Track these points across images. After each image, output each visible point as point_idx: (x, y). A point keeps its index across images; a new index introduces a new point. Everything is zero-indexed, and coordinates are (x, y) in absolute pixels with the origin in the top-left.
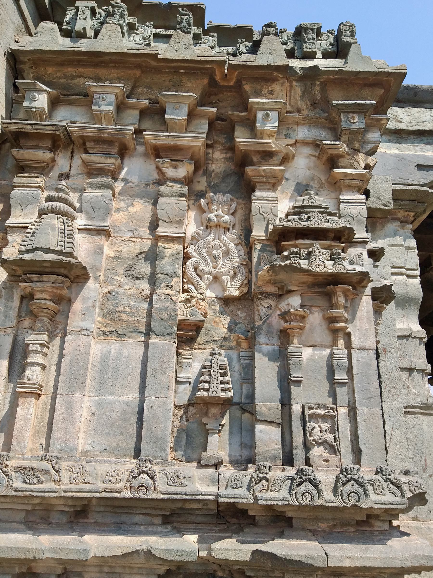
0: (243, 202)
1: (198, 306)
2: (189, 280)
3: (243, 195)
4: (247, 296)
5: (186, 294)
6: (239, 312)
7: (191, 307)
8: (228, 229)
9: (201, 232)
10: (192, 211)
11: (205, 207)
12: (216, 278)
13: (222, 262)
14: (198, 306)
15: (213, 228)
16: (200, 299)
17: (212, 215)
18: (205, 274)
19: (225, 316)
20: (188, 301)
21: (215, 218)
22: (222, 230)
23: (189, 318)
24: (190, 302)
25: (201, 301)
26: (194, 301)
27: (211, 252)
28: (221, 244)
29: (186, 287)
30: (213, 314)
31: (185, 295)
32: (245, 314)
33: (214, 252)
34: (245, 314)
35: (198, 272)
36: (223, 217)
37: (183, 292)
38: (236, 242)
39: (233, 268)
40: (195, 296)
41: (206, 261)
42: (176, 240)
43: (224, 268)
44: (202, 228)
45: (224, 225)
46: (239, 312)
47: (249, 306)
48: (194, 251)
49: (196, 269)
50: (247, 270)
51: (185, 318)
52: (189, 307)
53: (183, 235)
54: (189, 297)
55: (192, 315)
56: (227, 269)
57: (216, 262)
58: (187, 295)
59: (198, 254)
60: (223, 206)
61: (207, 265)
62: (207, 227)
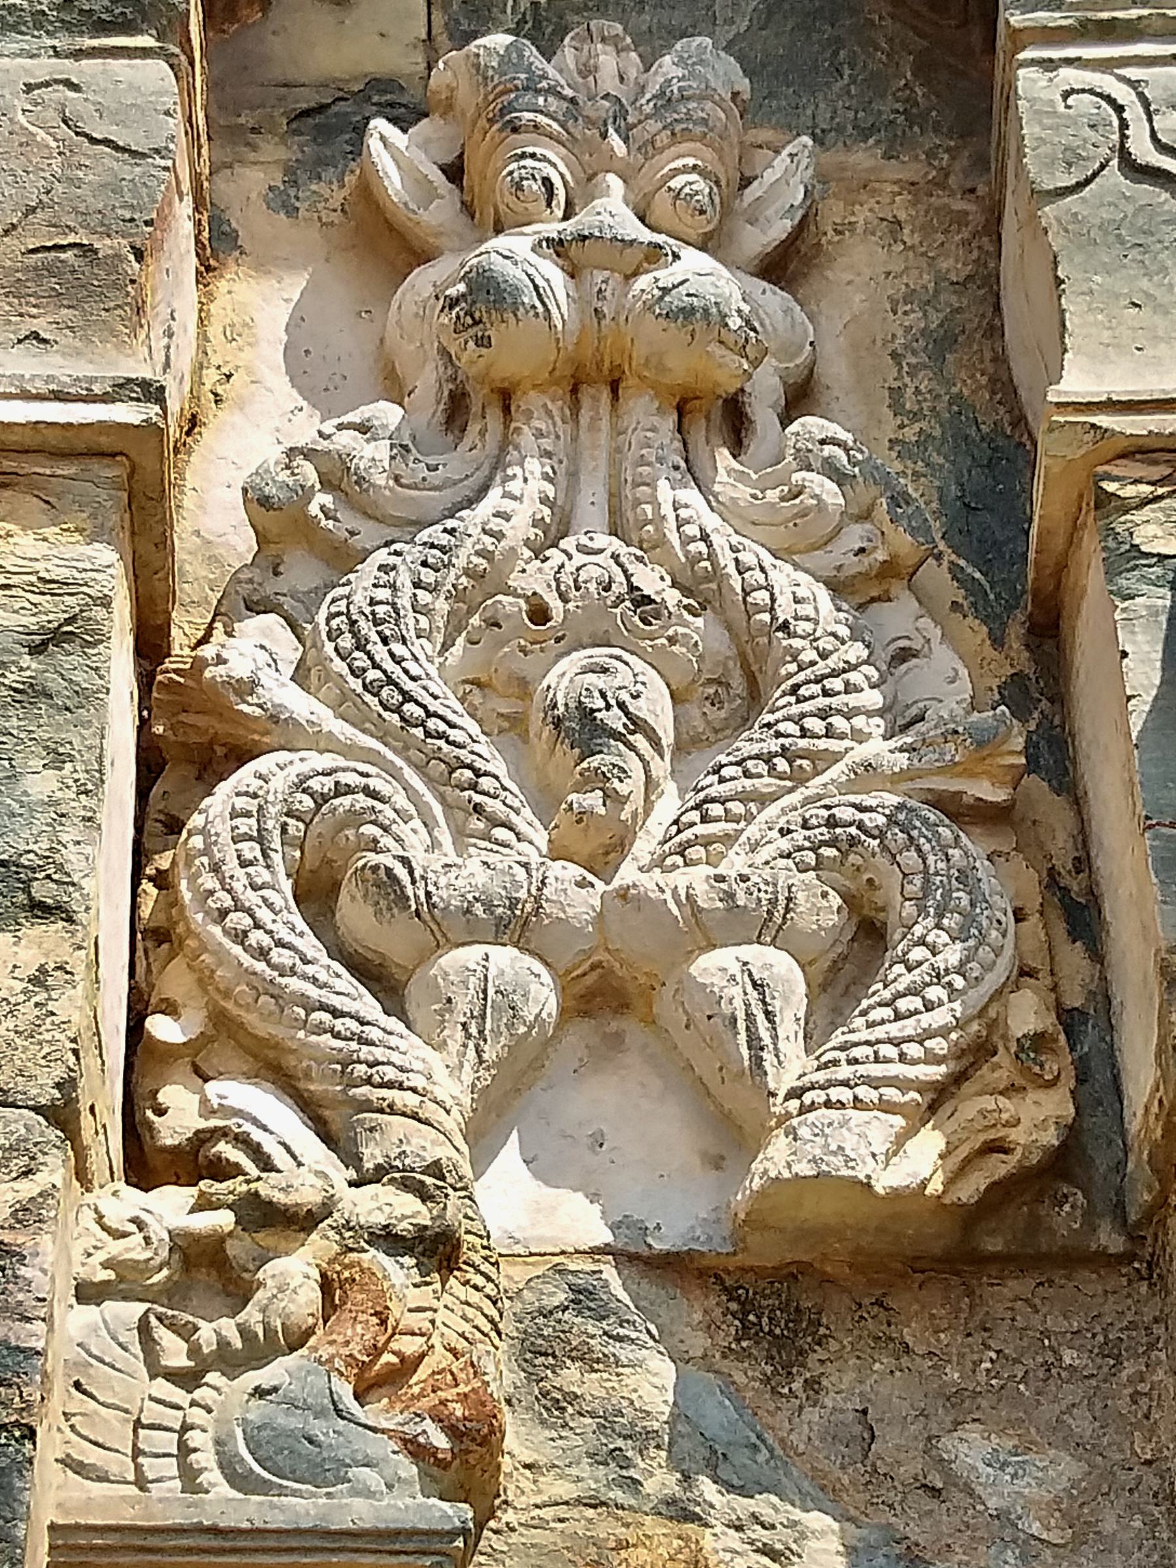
0: (895, 171)
1: (356, 1333)
2: (222, 1025)
3: (886, 107)
4: (1065, 1219)
5: (185, 1195)
6: (971, 1450)
7: (257, 1350)
8: (735, 424)
9: (372, 456)
10: (262, 267)
11: (429, 194)
12: (606, 996)
13: (668, 806)
14: (356, 1333)
15: (531, 400)
16: (388, 1239)
17: (515, 254)
18: (446, 926)
19: (763, 1504)
20: (208, 1271)
21: (552, 273)
22: (649, 423)
23: (222, 1504)
24: (236, 1290)
25: (397, 1272)
26: (292, 1277)
27: (523, 687)
28: (650, 580)
29: (180, 1113)
30: (595, 1478)
31: (172, 1207)
32: (1066, 1469)
33: (564, 678)
34: (1066, 1469)
35: (354, 912)
36: (654, 255)
37: (144, 1165)
38: (841, 554)
39: (836, 847)
40: (307, 1195)
41: (453, 776)
42: (34, 486)
43: (721, 849)
44: (389, 414)
45: (681, 365)
46: (971, 1450)
47: (1112, 1353)
48: (300, 676)
49: (316, 894)
50: (1029, 882)
51: (166, 1503)
52: (231, 1361)
53: (126, 413)
54: (224, 1219)
55: (283, 1457)
56: (760, 854)
57: (598, 780)
58: (204, 1204)
59: (342, 704)
60: (649, 149)
61: (473, 819)
62: (456, 411)
